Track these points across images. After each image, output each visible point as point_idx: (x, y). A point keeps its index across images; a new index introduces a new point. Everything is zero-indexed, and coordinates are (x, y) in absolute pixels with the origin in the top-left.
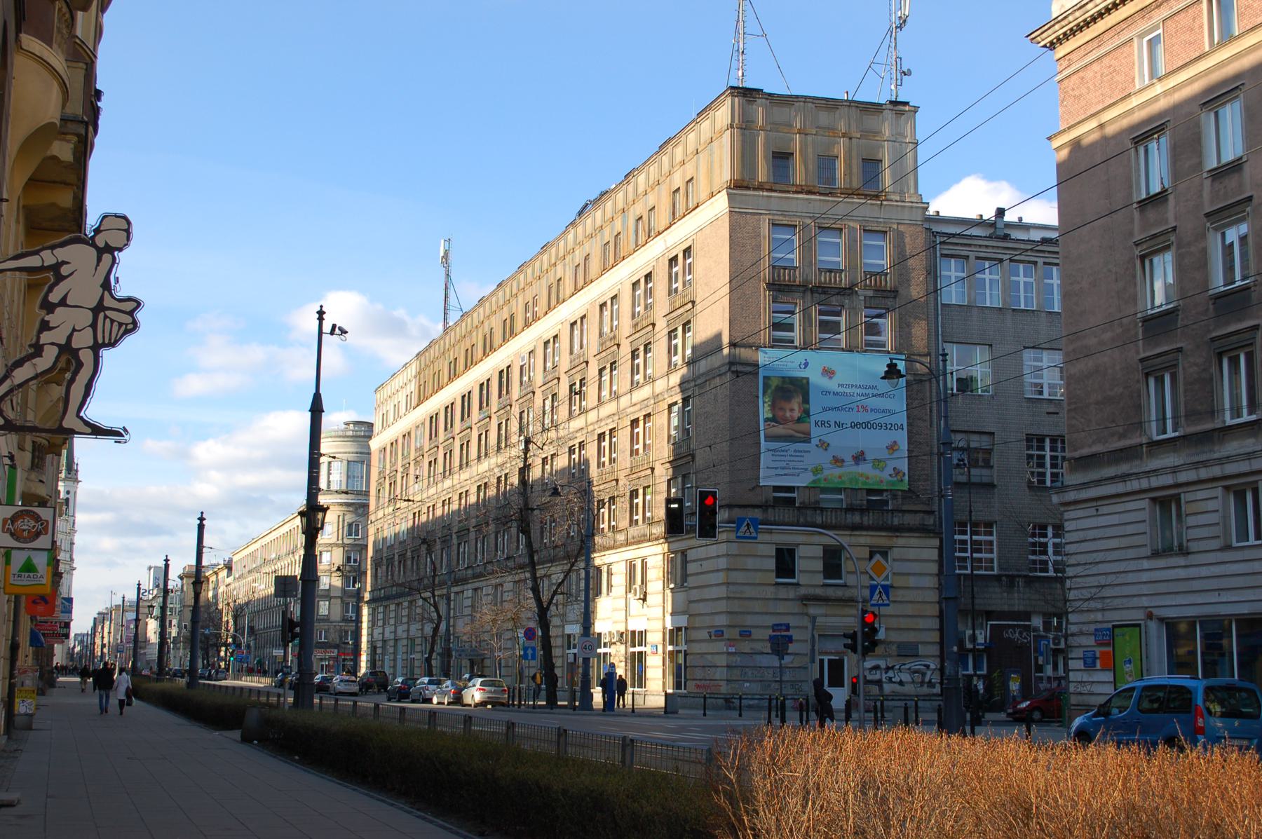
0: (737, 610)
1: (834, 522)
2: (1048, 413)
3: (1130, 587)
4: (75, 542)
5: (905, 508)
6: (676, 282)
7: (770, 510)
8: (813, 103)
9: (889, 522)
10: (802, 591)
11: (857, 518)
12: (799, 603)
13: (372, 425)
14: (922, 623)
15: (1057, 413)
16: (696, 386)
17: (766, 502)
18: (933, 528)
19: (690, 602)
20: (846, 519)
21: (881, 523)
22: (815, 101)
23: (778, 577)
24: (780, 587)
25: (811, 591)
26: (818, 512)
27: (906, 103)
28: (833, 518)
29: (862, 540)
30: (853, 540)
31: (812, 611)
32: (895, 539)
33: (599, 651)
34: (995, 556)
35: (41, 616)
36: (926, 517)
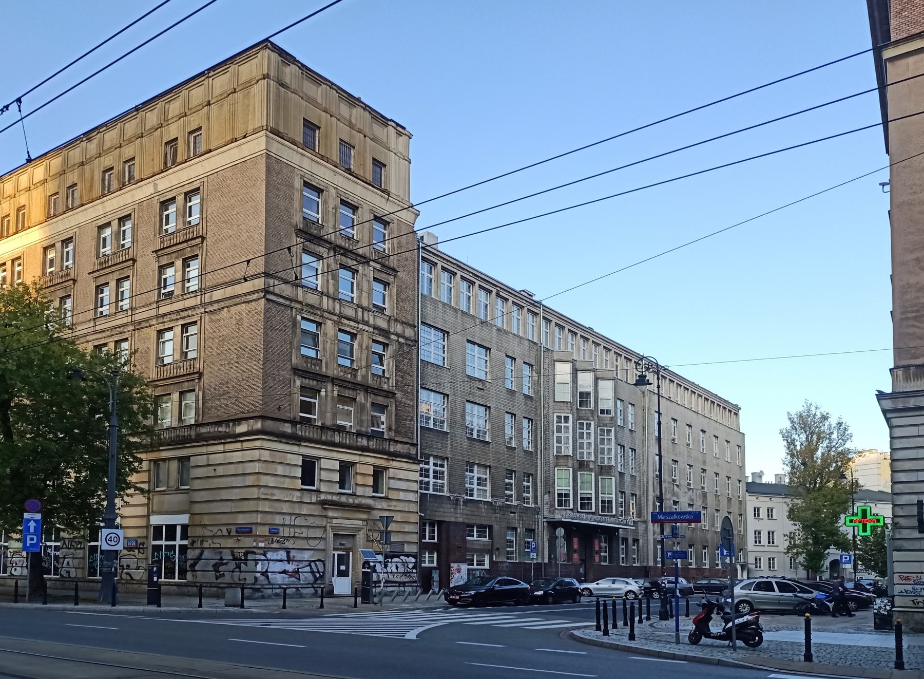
0: (267, 510)
1: (348, 442)
2: (478, 388)
3: (204, 505)
5: (397, 439)
6: (67, 261)
8: (337, 92)
9: (387, 448)
11: (364, 442)
12: (319, 507)
14: (407, 528)
15: (483, 390)
16: (205, 312)
17: (295, 418)
18: (414, 456)
19: (192, 502)
20: (357, 441)
21: (381, 448)
22: (339, 91)
23: (302, 484)
24: (305, 492)
25: (329, 497)
27: (404, 128)
28: (348, 440)
29: (369, 460)
30: (363, 459)
32: (391, 462)
34: (445, 482)
36: (412, 448)
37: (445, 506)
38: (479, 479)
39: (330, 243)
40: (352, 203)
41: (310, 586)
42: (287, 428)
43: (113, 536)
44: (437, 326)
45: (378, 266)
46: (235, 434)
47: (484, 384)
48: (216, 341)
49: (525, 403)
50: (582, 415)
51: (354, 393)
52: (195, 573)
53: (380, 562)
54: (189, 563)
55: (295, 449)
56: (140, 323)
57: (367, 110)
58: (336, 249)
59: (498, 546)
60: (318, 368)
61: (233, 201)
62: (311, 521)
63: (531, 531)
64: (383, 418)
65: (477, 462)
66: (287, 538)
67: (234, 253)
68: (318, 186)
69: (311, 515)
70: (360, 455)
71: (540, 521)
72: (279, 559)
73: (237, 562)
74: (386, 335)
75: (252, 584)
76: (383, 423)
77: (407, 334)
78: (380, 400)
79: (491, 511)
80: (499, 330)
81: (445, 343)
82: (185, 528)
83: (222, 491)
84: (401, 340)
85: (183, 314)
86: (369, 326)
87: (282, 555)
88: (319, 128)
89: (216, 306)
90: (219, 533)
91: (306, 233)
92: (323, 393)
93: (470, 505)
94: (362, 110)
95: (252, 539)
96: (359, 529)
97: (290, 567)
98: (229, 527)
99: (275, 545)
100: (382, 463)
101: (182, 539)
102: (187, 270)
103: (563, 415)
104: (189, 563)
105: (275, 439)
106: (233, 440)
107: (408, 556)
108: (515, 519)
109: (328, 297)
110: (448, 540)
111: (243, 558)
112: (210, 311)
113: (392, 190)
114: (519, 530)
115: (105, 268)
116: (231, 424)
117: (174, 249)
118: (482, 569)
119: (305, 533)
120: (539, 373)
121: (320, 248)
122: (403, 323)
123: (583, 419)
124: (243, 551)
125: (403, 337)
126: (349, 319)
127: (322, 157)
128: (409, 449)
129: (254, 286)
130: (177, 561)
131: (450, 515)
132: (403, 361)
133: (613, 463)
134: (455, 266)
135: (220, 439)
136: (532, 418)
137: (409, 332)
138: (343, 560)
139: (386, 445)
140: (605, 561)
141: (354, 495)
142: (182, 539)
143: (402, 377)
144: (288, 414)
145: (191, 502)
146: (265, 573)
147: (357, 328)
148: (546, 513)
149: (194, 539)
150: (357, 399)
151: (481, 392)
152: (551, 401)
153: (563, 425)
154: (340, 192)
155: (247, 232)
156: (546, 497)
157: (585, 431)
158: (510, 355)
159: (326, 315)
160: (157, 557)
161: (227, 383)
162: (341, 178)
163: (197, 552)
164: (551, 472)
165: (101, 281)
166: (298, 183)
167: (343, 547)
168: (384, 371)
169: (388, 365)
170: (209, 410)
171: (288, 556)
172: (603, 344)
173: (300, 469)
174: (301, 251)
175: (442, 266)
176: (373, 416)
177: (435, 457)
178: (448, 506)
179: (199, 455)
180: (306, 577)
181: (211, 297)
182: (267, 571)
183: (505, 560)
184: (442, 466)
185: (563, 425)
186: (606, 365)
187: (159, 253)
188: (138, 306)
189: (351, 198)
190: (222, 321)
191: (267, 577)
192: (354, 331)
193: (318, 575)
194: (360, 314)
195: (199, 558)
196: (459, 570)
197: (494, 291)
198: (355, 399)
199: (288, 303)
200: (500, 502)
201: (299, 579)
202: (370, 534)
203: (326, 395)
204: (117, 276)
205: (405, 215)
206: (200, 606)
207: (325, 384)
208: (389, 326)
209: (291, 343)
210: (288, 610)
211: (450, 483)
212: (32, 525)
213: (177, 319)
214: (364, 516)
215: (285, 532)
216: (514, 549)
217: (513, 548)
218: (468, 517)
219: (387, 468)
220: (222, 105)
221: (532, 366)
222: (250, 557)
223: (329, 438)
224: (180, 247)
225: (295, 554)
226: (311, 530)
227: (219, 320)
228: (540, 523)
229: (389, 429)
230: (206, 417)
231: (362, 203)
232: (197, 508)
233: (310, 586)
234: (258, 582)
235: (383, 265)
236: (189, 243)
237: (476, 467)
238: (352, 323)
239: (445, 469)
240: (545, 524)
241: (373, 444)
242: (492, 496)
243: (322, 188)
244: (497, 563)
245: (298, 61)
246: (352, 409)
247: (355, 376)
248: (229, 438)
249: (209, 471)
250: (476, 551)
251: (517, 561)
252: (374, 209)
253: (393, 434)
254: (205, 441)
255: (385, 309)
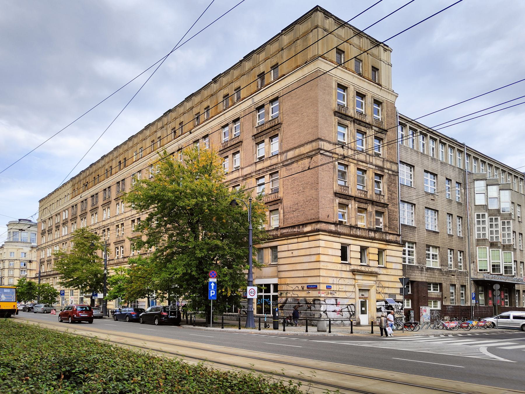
3: (287, 273)
4: (39, 203)
5: (390, 232)
7: (338, 226)
8: (353, 30)
9: (385, 238)
10: (352, 267)
11: (372, 234)
12: (351, 273)
13: (519, 290)
17: (336, 222)
24: (343, 265)
25: (356, 268)
26: (358, 230)
27: (387, 46)
31: (357, 277)
33: (432, 302)
35: (409, 292)
36: (398, 237)
37: (416, 272)
38: (433, 255)
39: (352, 118)
40: (362, 93)
41: (348, 319)
42: (332, 228)
43: (252, 290)
44: (408, 163)
45: (377, 129)
46: (304, 232)
47: (434, 197)
48: (290, 181)
49: (458, 207)
50: (492, 213)
51: (366, 205)
52: (283, 311)
53: (383, 306)
54: (279, 305)
55: (337, 239)
56: (246, 175)
57: (368, 38)
58: (355, 121)
59: (446, 296)
60: (347, 192)
61: (298, 100)
62: (347, 281)
63: (463, 286)
64: (381, 220)
65: (432, 244)
66: (335, 291)
67: (299, 130)
68: (345, 85)
69: (347, 278)
70: (371, 242)
71: (469, 280)
72: (332, 303)
73: (309, 305)
74: (382, 170)
75: (319, 318)
76: (381, 223)
77: (393, 169)
78: (379, 209)
79: (441, 275)
80: (441, 163)
81: (412, 173)
82: (276, 286)
83: (297, 264)
84: (390, 172)
85: (270, 168)
86: (373, 165)
87: (333, 301)
88: (344, 52)
89: (289, 162)
90: (297, 289)
91: (339, 113)
92: (350, 206)
93: (429, 271)
94: (366, 39)
95: (317, 292)
96: (372, 286)
97: (338, 308)
98: (303, 285)
99: (330, 296)
100: (382, 246)
101: (274, 292)
102: (271, 143)
103: (481, 214)
104: (279, 305)
105: (327, 234)
106: (303, 236)
107: (398, 302)
108: (454, 280)
109: (351, 149)
110: (418, 292)
111: (312, 303)
112: (286, 165)
113: (383, 84)
114: (457, 286)
115: (226, 148)
116: (301, 227)
117: (265, 132)
118: (437, 310)
119: (344, 288)
120: (465, 188)
121: (346, 121)
122: (391, 162)
123: (493, 216)
124: (312, 299)
125: (391, 170)
126: (362, 162)
127: (346, 69)
128: (397, 238)
129: (312, 147)
130: (271, 304)
131: (418, 277)
132: (391, 185)
133: (512, 243)
134: (416, 126)
135: (296, 236)
136: (462, 216)
137: (394, 167)
138: (363, 304)
139: (384, 236)
140: (507, 305)
141: (368, 266)
142: (274, 292)
143: (391, 195)
144: (333, 220)
145: (279, 271)
146: (325, 312)
147: (367, 167)
148: (472, 276)
149: (281, 292)
150: (368, 209)
151: (433, 202)
152: (473, 205)
153: (481, 220)
154: (356, 88)
155: (307, 116)
156: (472, 265)
157: (494, 223)
158: (448, 178)
159: (350, 160)
160: (260, 302)
161: (297, 204)
162: (356, 79)
163: (284, 299)
164: (474, 250)
165: (225, 155)
166: (334, 85)
167: (363, 297)
168: (380, 191)
169: (383, 188)
170: (287, 220)
171: (336, 302)
172: (501, 168)
173: (340, 251)
174: (337, 124)
175: (410, 127)
176: (376, 219)
177: (409, 242)
178: (418, 272)
179: (283, 246)
180: (346, 315)
181: (286, 156)
182: (326, 311)
183: (450, 304)
184: (412, 248)
185: (481, 220)
186: (503, 181)
187: (256, 136)
188: (244, 166)
189: (361, 90)
190: (293, 170)
191: (327, 314)
192: (365, 169)
193: (352, 313)
194: (368, 158)
195: (285, 303)
196: (425, 311)
197: (438, 139)
198: (366, 209)
199: (331, 155)
200: (445, 269)
201: (342, 315)
202: (377, 289)
203: (352, 208)
204: (232, 152)
205: (390, 98)
206: (307, 331)
207: (350, 201)
208: (383, 164)
209: (333, 179)
210: (354, 334)
211: (418, 258)
212: (213, 285)
213: (267, 171)
214: (375, 279)
215: (334, 288)
216: (454, 298)
217: (453, 297)
218: (429, 278)
219: (384, 250)
220: (291, 48)
221: (461, 184)
222: (316, 302)
223: (354, 233)
224: (268, 131)
225: (340, 301)
226: (347, 286)
227: (291, 169)
228: (469, 282)
229: (385, 226)
230: (286, 223)
231: (367, 93)
232: (283, 275)
233: (348, 319)
234: (322, 317)
235: (380, 128)
236: (273, 128)
237: (431, 248)
238: (364, 164)
239: (414, 250)
240: (472, 282)
241: (377, 236)
242: (441, 265)
243: (346, 86)
244: (445, 306)
245: (333, 15)
246: (365, 215)
247: (366, 195)
248: (301, 234)
249: (289, 254)
250: (433, 299)
251: (457, 305)
252: (374, 96)
253: (387, 229)
254: (286, 237)
255: (380, 154)
